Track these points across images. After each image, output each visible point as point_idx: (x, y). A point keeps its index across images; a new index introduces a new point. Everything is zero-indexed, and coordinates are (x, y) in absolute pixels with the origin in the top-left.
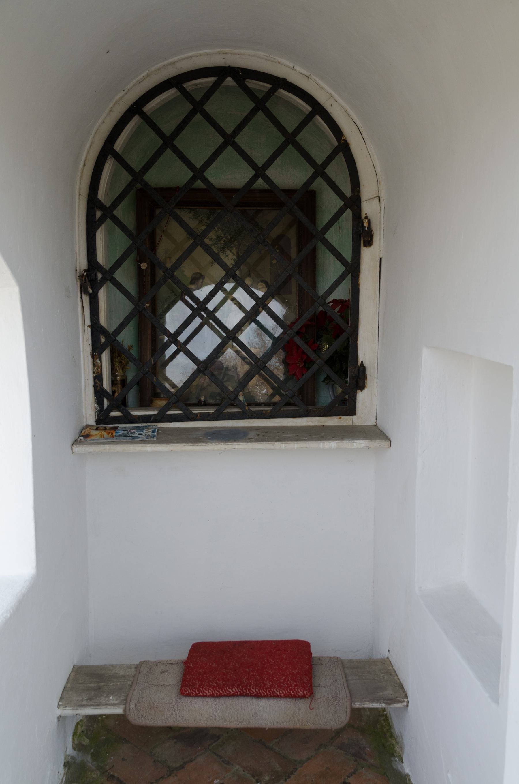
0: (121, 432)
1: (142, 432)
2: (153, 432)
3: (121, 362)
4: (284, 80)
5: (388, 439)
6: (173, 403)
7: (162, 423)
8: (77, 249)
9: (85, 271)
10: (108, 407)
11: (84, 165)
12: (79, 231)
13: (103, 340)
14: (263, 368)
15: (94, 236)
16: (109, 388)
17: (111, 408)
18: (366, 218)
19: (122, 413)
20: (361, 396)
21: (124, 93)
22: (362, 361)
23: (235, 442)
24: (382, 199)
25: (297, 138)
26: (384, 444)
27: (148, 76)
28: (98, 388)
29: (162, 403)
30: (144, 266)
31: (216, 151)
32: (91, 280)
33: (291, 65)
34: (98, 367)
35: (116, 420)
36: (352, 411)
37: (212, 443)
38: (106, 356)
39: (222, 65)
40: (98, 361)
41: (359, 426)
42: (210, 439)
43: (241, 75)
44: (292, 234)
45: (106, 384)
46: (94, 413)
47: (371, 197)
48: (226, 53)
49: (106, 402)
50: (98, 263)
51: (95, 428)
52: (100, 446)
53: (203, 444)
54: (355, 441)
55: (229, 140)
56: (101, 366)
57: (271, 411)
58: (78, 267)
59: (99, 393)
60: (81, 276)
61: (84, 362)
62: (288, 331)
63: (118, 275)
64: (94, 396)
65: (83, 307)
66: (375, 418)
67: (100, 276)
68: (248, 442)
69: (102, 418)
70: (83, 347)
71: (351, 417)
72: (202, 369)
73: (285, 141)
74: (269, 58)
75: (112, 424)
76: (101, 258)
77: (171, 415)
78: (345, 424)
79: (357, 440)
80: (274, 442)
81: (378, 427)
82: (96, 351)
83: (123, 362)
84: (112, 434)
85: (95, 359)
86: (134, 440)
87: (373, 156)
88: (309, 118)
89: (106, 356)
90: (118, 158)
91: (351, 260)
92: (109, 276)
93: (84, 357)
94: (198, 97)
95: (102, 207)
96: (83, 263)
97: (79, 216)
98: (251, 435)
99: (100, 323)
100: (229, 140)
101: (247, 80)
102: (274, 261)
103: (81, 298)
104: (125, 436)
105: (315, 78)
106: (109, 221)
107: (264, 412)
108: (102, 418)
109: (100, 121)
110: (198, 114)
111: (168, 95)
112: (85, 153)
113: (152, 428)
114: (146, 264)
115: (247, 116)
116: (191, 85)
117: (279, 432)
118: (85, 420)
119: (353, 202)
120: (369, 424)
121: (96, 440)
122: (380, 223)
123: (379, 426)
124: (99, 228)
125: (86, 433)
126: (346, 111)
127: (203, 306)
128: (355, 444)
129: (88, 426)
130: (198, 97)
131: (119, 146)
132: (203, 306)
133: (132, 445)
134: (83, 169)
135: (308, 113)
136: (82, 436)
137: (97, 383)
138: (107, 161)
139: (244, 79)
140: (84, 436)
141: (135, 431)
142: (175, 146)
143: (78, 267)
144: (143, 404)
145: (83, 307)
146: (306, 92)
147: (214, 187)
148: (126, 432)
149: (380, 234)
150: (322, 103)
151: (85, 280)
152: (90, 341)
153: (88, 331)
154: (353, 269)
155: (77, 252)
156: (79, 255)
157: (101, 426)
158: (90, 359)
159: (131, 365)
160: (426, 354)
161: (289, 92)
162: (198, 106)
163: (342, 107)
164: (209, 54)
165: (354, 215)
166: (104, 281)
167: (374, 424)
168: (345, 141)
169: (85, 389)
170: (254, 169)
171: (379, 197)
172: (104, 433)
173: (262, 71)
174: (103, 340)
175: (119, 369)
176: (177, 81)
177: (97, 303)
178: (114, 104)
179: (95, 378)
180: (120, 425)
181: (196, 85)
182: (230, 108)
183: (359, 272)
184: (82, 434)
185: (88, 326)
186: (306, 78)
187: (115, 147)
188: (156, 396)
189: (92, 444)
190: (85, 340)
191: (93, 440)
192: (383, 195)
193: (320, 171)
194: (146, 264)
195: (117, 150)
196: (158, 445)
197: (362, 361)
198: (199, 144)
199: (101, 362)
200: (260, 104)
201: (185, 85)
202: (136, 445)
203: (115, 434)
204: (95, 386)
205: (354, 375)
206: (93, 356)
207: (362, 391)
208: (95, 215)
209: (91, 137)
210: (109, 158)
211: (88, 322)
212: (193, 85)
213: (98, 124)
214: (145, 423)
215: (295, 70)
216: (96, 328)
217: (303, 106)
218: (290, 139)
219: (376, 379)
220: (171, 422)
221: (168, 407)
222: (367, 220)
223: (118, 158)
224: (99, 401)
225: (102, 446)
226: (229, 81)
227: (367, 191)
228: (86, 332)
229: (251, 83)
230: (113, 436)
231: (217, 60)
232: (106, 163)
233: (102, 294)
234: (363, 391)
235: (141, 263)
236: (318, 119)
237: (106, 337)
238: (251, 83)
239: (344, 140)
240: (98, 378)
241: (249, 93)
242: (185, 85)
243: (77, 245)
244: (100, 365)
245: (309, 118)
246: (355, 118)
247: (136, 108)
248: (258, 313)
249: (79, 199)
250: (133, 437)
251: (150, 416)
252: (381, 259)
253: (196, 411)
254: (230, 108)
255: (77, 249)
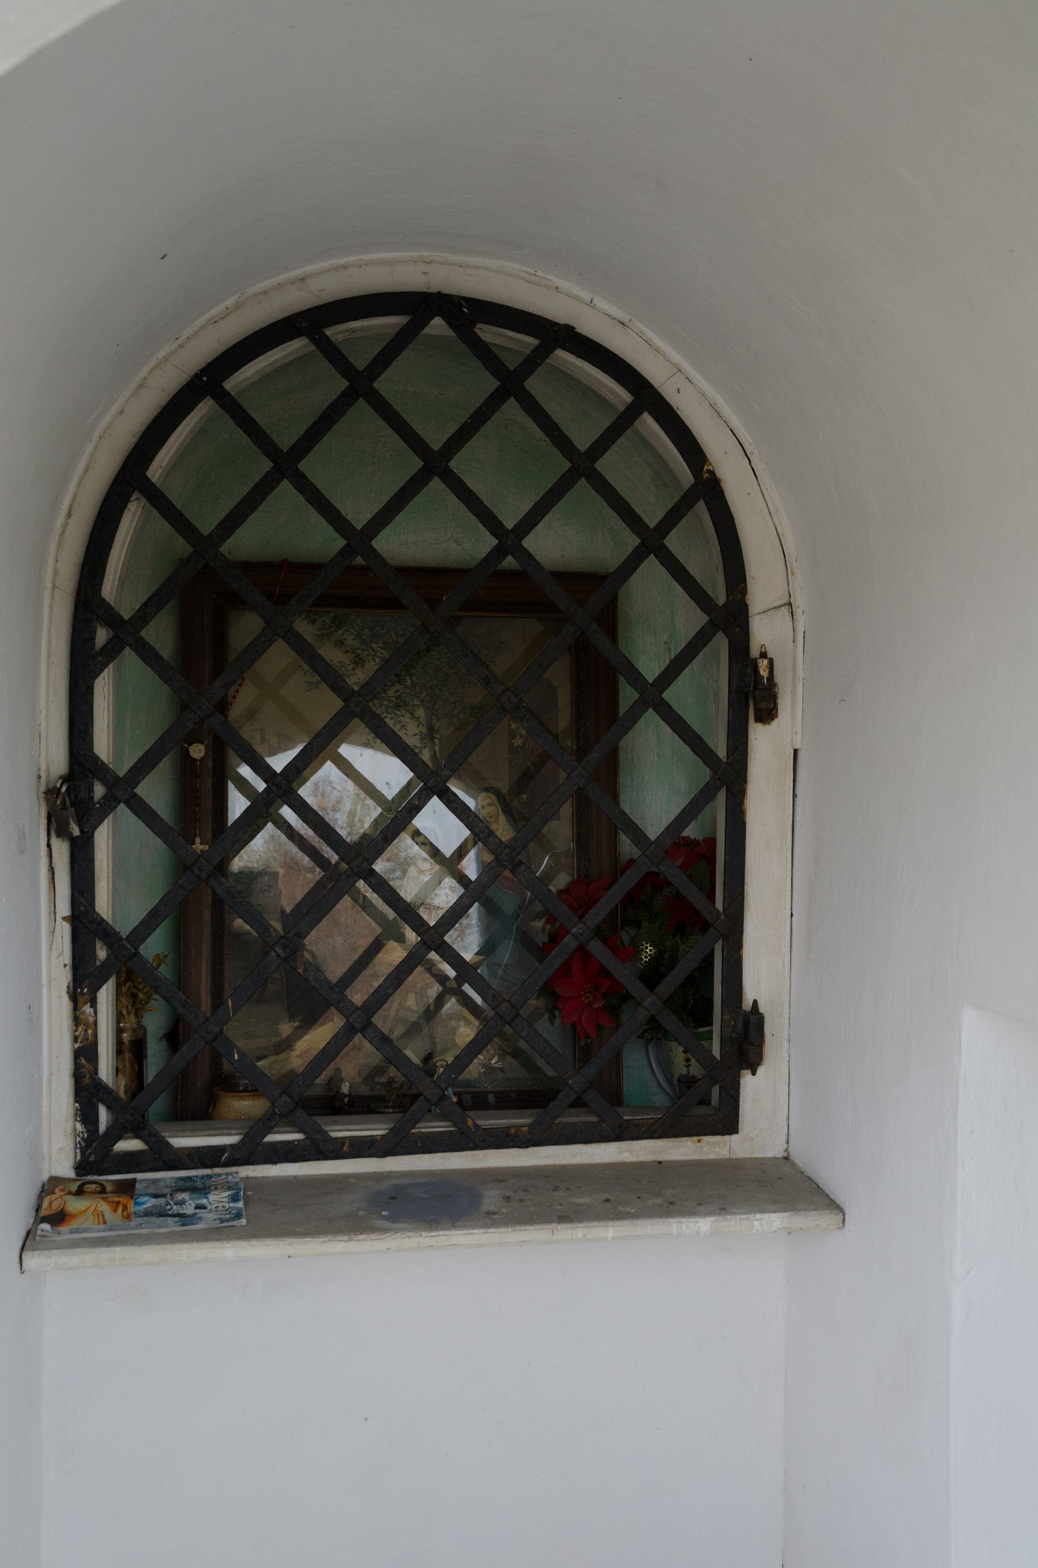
0: (150, 1203)
1: (204, 1201)
2: (234, 1199)
3: (134, 996)
4: (569, 329)
5: (834, 1206)
6: (282, 1116)
7: (251, 1167)
8: (43, 724)
9: (66, 779)
10: (108, 1128)
11: (69, 515)
12: (48, 676)
13: (102, 953)
14: (514, 1019)
15: (90, 690)
16: (110, 1077)
17: (116, 1132)
18: (763, 655)
19: (146, 1143)
20: (752, 1087)
21: (177, 343)
22: (755, 1002)
23: (454, 1227)
24: (798, 613)
25: (599, 465)
26: (827, 1219)
27: (238, 306)
28: (87, 1080)
29: (246, 1106)
30: (197, 751)
31: (403, 490)
32: (75, 801)
33: (586, 296)
34: (87, 1025)
35: (131, 1162)
36: (727, 1122)
37: (396, 1231)
38: (106, 995)
39: (422, 289)
40: (87, 1009)
41: (745, 1159)
42: (387, 1218)
43: (466, 313)
44: (560, 674)
45: (105, 1069)
46: (72, 1146)
47: (772, 605)
48: (431, 262)
49: (103, 1115)
50: (96, 758)
51: (74, 1187)
52: (97, 1250)
53: (374, 1236)
54: (758, 1216)
55: (435, 465)
56: (96, 1023)
57: (531, 1126)
58: (43, 767)
59: (87, 1092)
60: (51, 793)
61: (50, 1012)
62: (575, 925)
63: (144, 789)
64: (72, 1099)
65: (52, 871)
66: (784, 1138)
67: (99, 791)
68: (488, 1226)
69: (92, 1158)
70: (49, 974)
71: (727, 1137)
72: (358, 1026)
73: (570, 470)
74: (534, 278)
75: (120, 1173)
76: (102, 745)
77: (275, 1144)
78: (711, 1156)
79: (762, 1212)
80: (555, 1225)
81: (794, 1165)
82: (83, 984)
83: (141, 996)
84: (125, 1207)
85: (80, 1003)
86: (186, 1228)
87: (777, 510)
88: (626, 419)
89: (106, 995)
90: (157, 499)
91: (725, 754)
92: (123, 791)
93: (50, 1002)
94: (361, 361)
95: (113, 620)
96: (55, 758)
97: (49, 641)
98: (491, 1199)
99: (97, 909)
100: (435, 465)
101: (479, 325)
102: (518, 742)
103: (49, 846)
104: (162, 1214)
105: (643, 328)
106: (129, 655)
107: (513, 1131)
108: (94, 1158)
109: (114, 409)
110: (361, 399)
111: (281, 355)
112: (72, 486)
113: (229, 1188)
114: (202, 747)
115: (480, 407)
116: (340, 332)
117: (556, 1189)
118: (46, 1164)
119: (729, 616)
120: (770, 1154)
121: (85, 1230)
122: (794, 667)
123: (797, 1161)
124: (102, 670)
125: (56, 1206)
126: (713, 406)
127: (365, 866)
128: (756, 1223)
129: (52, 1185)
130: (361, 361)
131: (160, 471)
132: (365, 866)
133: (185, 1246)
134: (65, 526)
135: (622, 408)
136: (44, 1220)
137: (83, 1067)
138: (129, 505)
139: (473, 323)
140: (50, 1217)
141: (185, 1196)
142: (302, 476)
143: (43, 767)
144: (198, 1112)
145: (52, 871)
146: (621, 359)
147: (383, 561)
148: (162, 1201)
149: (794, 692)
150: (656, 383)
151: (63, 803)
152: (67, 957)
153: (65, 930)
154: (729, 776)
155: (43, 729)
156: (47, 737)
157: (90, 1178)
158: (66, 1004)
159: (157, 1003)
160: (973, 1026)
161: (578, 356)
162: (360, 385)
163: (703, 395)
164: (391, 263)
165: (732, 646)
166: (109, 804)
167: (781, 1154)
168: (712, 473)
169: (50, 1082)
170: (495, 535)
171: (790, 604)
172: (104, 1207)
173: (516, 306)
174: (102, 953)
175: (129, 1014)
176: (311, 322)
177: (91, 860)
178: (151, 371)
179: (77, 1054)
180: (139, 1176)
181: (354, 330)
182: (432, 387)
183: (745, 782)
184: (43, 1212)
185: (64, 918)
186: (619, 326)
187: (149, 473)
188: (225, 1083)
189: (75, 1244)
190: (55, 953)
191: (77, 1231)
192: (800, 601)
193: (652, 543)
194: (202, 747)
195: (154, 481)
196: (254, 1242)
197: (755, 1002)
198: (358, 472)
199: (96, 1013)
200: (511, 383)
201: (329, 332)
202: (195, 1245)
203: (132, 1208)
204: (77, 1076)
205: (734, 1035)
206: (74, 996)
207: (754, 1073)
208: (92, 638)
209: (90, 448)
210: (133, 498)
211: (64, 908)
212: (346, 331)
213: (107, 418)
214: (205, 1167)
215: (594, 307)
216: (84, 924)
217: (610, 390)
218: (582, 467)
219: (785, 1044)
220: (275, 1163)
221: (267, 1123)
222: (766, 662)
223: (157, 499)
224: (86, 1114)
225: (104, 1249)
226: (437, 325)
227: (763, 589)
228: (58, 932)
229: (488, 333)
230: (128, 1217)
231: (409, 277)
232: (126, 512)
233: (103, 836)
234: (761, 1070)
235: (190, 745)
236: (648, 422)
237: (110, 947)
238: (488, 333)
239: (709, 471)
240: (85, 1054)
241: (485, 354)
242: (329, 332)
243: (44, 713)
244: (91, 1019)
245: (626, 419)
246: (736, 423)
247: (207, 382)
248: (415, 809)
249: (53, 597)
250: (184, 1219)
251: (220, 1149)
252: (796, 751)
253: (340, 1131)
254: (432, 387)
255: (43, 724)
